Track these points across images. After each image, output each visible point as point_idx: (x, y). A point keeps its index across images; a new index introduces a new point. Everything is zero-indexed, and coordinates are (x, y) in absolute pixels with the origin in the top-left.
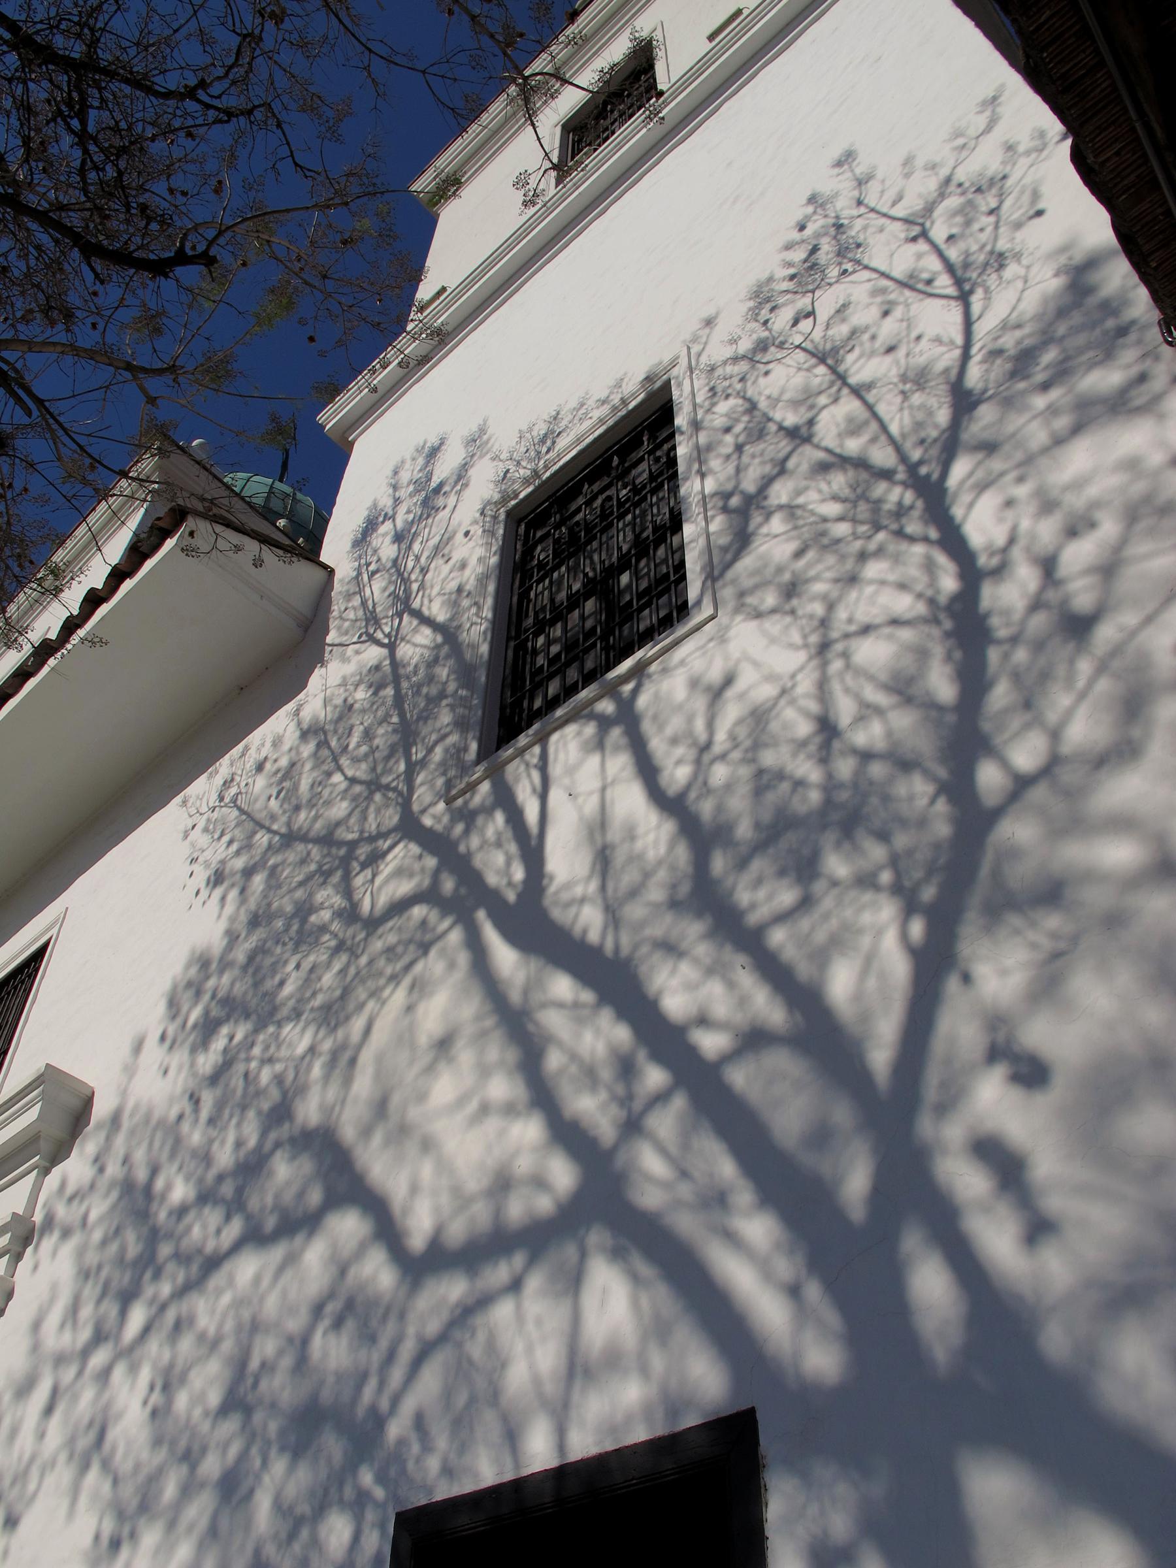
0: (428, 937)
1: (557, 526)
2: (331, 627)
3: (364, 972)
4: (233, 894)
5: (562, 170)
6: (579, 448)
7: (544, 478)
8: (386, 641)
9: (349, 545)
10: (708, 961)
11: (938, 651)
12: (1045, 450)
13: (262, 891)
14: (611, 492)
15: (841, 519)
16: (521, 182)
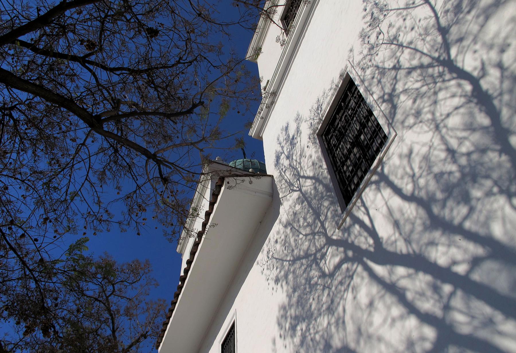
0: (351, 273)
1: (334, 132)
2: (279, 192)
3: (335, 292)
4: (284, 283)
5: (287, 30)
6: (329, 106)
7: (323, 119)
8: (298, 189)
9: (274, 166)
10: (447, 242)
11: (476, 110)
12: (480, 31)
13: (293, 280)
14: (346, 113)
15: (423, 86)
16: (278, 40)
